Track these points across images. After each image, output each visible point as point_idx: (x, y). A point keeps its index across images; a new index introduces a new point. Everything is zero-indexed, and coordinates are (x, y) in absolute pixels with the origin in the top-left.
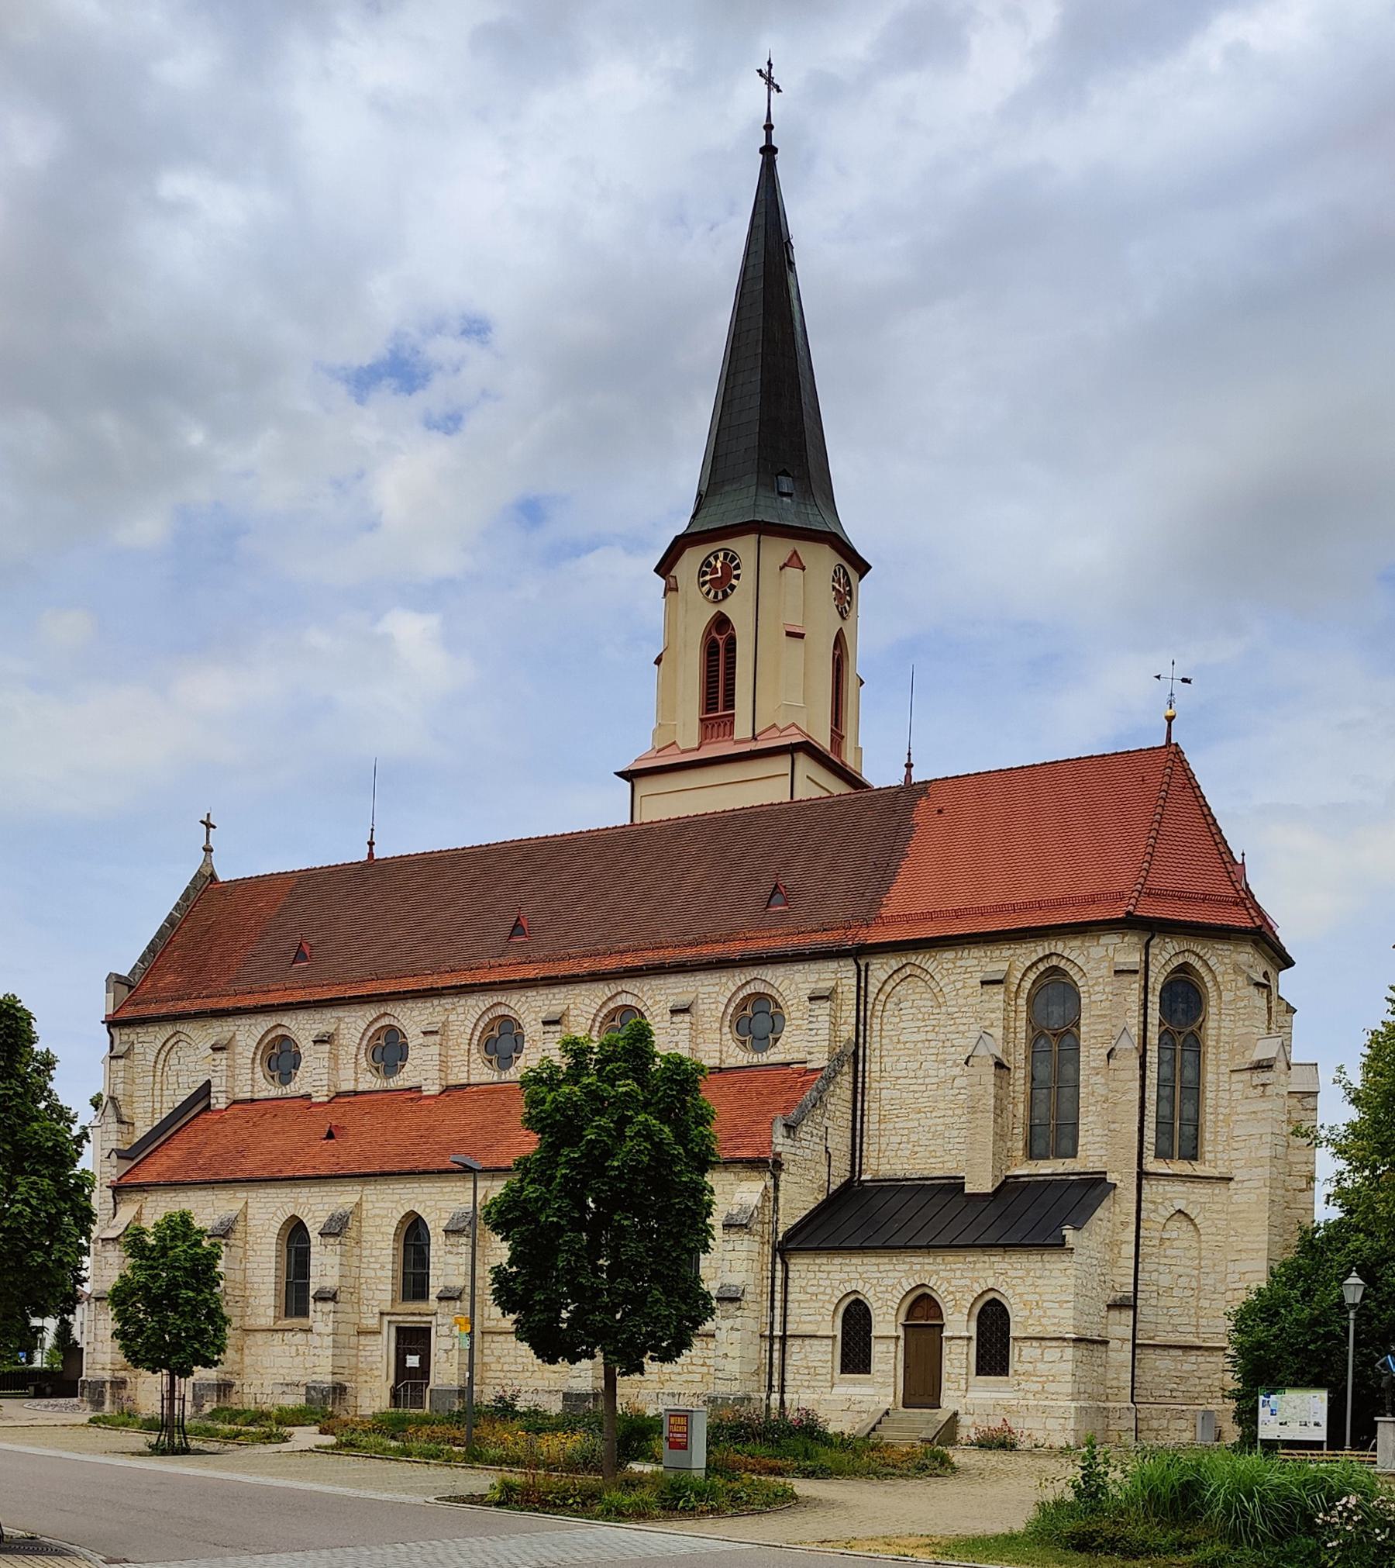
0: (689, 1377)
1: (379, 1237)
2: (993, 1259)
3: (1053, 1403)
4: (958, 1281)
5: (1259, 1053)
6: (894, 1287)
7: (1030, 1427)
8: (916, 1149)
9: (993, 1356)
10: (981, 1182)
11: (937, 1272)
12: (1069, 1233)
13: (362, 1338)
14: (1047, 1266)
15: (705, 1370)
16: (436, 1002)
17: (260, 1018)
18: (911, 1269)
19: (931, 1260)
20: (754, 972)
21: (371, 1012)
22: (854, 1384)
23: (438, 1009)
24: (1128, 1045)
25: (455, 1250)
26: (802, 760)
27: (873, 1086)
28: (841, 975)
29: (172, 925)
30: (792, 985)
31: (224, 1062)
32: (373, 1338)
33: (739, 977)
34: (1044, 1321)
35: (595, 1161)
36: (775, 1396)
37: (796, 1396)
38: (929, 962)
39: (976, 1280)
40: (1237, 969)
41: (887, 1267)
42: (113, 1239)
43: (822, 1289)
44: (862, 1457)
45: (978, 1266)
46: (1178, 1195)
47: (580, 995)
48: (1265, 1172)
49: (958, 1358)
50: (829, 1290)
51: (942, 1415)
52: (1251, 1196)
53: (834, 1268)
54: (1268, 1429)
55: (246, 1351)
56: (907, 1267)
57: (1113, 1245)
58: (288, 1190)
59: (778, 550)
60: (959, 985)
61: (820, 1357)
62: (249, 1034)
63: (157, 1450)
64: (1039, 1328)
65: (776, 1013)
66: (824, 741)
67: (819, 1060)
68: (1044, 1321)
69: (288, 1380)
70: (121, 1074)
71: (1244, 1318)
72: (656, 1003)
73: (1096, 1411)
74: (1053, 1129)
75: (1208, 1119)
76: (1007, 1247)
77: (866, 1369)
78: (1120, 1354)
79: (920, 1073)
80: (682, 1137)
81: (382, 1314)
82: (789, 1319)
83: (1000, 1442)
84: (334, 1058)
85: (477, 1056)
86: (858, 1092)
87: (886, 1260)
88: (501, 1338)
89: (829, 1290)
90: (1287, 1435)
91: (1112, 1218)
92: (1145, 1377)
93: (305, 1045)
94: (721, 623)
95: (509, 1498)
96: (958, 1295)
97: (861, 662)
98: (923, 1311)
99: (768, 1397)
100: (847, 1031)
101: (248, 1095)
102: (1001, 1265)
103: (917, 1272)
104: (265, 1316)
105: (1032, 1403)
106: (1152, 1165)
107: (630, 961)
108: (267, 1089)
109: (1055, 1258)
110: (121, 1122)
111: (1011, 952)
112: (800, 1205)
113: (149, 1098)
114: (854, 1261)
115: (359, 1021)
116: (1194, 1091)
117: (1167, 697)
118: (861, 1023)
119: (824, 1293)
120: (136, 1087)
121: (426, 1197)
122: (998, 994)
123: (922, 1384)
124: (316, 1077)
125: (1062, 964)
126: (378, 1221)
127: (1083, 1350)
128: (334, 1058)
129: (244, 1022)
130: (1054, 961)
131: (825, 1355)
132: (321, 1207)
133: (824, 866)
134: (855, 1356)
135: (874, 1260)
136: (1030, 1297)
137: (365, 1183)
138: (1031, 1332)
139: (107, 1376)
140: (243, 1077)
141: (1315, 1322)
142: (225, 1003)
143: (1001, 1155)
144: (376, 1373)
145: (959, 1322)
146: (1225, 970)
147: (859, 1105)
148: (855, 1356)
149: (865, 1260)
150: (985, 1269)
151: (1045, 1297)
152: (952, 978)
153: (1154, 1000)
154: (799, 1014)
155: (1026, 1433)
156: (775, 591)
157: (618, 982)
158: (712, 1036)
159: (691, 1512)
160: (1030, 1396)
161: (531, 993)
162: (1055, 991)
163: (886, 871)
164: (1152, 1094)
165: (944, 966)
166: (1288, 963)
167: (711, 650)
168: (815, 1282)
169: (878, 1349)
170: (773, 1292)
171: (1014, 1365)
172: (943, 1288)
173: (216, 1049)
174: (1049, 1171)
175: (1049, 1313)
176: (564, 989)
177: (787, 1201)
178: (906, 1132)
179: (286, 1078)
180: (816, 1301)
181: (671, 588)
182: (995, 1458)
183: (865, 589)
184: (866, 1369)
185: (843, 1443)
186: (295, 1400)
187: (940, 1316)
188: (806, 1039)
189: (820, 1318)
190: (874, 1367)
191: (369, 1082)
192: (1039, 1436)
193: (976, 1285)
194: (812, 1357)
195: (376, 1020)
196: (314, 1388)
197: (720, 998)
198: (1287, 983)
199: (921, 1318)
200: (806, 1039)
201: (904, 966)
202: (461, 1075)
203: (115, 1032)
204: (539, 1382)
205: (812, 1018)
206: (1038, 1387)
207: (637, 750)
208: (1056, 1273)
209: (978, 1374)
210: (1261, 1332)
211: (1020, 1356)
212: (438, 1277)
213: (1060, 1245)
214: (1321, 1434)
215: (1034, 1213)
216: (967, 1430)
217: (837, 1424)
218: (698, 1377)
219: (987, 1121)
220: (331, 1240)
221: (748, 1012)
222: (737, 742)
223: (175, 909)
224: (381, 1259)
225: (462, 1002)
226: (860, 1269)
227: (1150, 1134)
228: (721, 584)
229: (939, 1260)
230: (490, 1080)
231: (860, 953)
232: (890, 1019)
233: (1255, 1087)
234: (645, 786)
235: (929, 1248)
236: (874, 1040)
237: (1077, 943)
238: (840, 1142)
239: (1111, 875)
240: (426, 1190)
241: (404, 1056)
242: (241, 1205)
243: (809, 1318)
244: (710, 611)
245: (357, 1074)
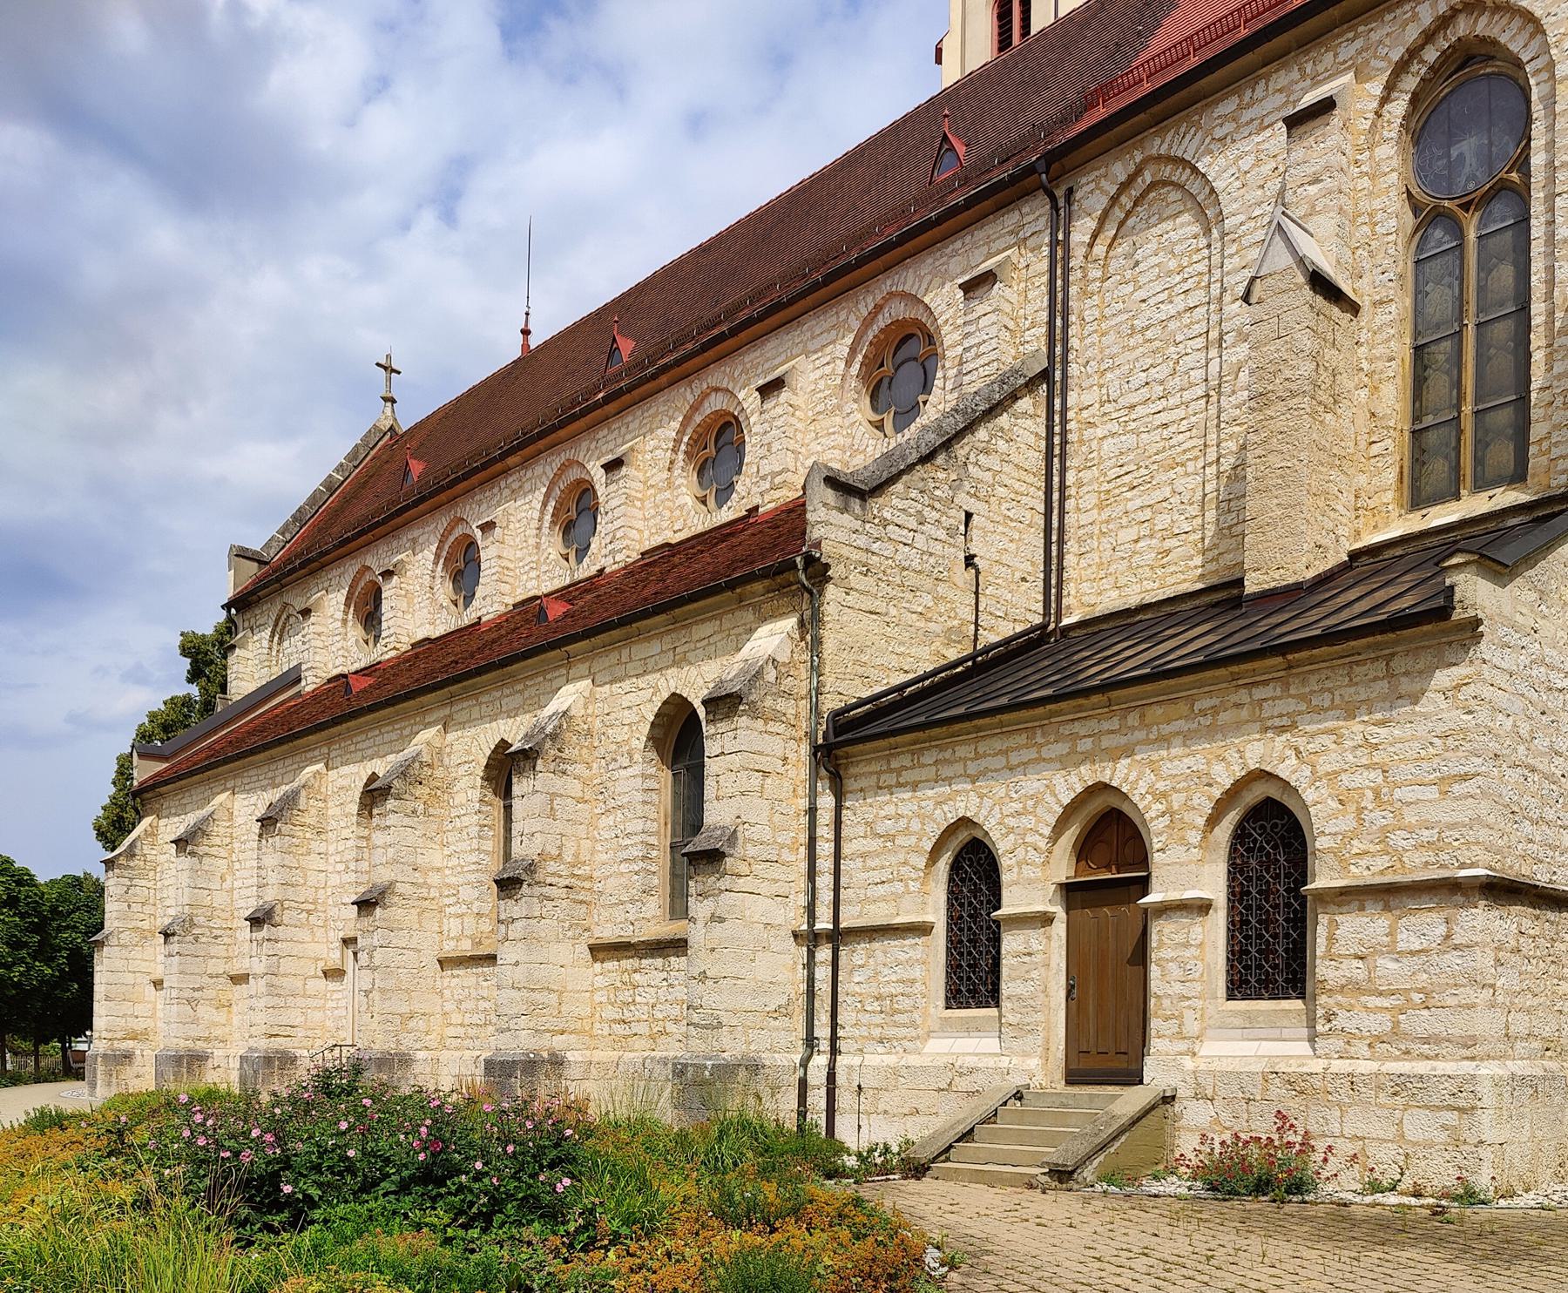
3: (1422, 1067)
8: (1168, 544)
9: (1271, 957)
18: (1073, 751)
19: (1115, 724)
36: (820, 1061)
37: (857, 1061)
43: (902, 823)
45: (1224, 717)
49: (1189, 958)
50: (915, 825)
64: (1382, 862)
68: (1398, 839)
82: (843, 894)
86: (1055, 451)
87: (1021, 739)
89: (915, 825)
96: (1177, 800)
99: (804, 1064)
105: (1365, 1067)
111: (1358, 44)
112: (895, 662)
119: (906, 832)
138: (1360, 874)
145: (1190, 868)
147: (1056, 479)
155: (1345, 1148)
170: (812, 841)
171: (1324, 969)
172: (1143, 787)
175: (1410, 817)
177: (842, 647)
178: (1148, 514)
184: (992, 996)
187: (1143, 860)
189: (900, 887)
190: (1006, 989)
201: (1139, 171)
206: (1378, 1024)
211: (1339, 943)
221: (888, 367)
223: (337, 470)
225: (529, 474)
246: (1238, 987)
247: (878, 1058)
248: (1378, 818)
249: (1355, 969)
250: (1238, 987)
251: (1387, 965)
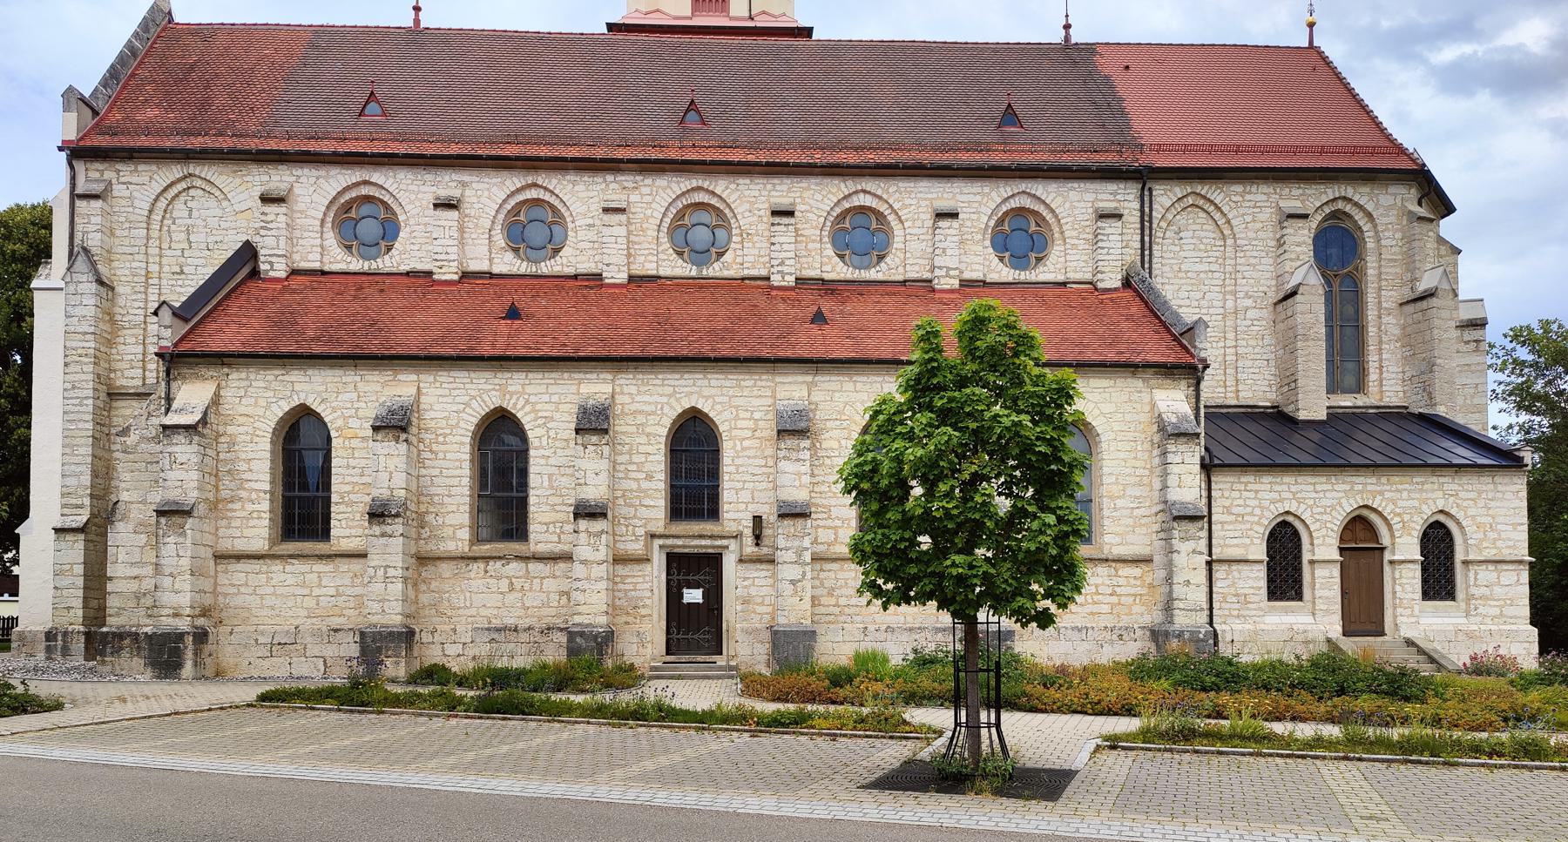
0: (1095, 609)
1: (643, 439)
2: (1442, 480)
3: (1514, 627)
6: (1333, 508)
9: (1439, 578)
11: (1381, 493)
13: (619, 568)
14: (1500, 488)
15: (1114, 599)
16: (610, 178)
17: (334, 171)
20: (1023, 185)
21: (513, 181)
22: (1286, 611)
23: (612, 186)
25: (794, 455)
28: (1124, 197)
29: (134, 55)
30: (1072, 205)
31: (282, 218)
32: (637, 567)
34: (1499, 544)
39: (1425, 501)
41: (1326, 487)
42: (187, 427)
43: (1249, 510)
47: (808, 189)
53: (1263, 487)
55: (423, 587)
56: (1348, 487)
58: (487, 375)
60: (1248, 218)
61: (1251, 583)
64: (1494, 552)
65: (1037, 232)
68: (1499, 544)
69: (496, 623)
70: (98, 219)
72: (906, 206)
77: (1451, 595)
79: (1203, 302)
81: (653, 536)
87: (1324, 479)
88: (835, 566)
96: (1406, 517)
98: (1361, 539)
101: (316, 265)
102: (1452, 486)
103: (1360, 492)
104: (454, 538)
109: (1507, 480)
110: (100, 282)
113: (141, 257)
114: (1287, 479)
115: (495, 190)
117: (1307, 7)
118: (1146, 249)
119: (1252, 514)
120: (117, 241)
121: (714, 391)
123: (1363, 607)
124: (439, 249)
125: (1348, 208)
126: (640, 419)
130: (1340, 205)
132: (546, 398)
135: (1310, 479)
136: (1483, 520)
137: (620, 371)
139: (183, 625)
144: (643, 612)
145: (1405, 547)
149: (1300, 479)
150: (1433, 491)
151: (1500, 519)
152: (1241, 211)
154: (1075, 233)
157: (857, 180)
158: (974, 248)
160: (1488, 620)
161: (743, 181)
168: (1241, 502)
173: (266, 199)
174: (1349, 404)
175: (1503, 535)
176: (787, 181)
180: (1243, 522)
184: (1451, 595)
185: (1048, 682)
186: (554, 653)
189: (1248, 541)
193: (1424, 507)
194: (1241, 584)
195: (518, 191)
196: (582, 634)
197: (983, 209)
199: (1365, 541)
202: (648, 266)
203: (80, 166)
208: (1509, 496)
212: (737, 491)
218: (1106, 609)
220: (594, 439)
222: (731, 19)
224: (647, 467)
226: (1293, 488)
229: (1384, 480)
230: (687, 274)
233: (1467, 342)
237: (1365, 189)
240: (713, 383)
242: (413, 391)
243: (1235, 541)
246: (1426, 595)
247: (1238, 626)
248: (1492, 535)
249: (1483, 590)
250: (1426, 595)
251: (1497, 589)
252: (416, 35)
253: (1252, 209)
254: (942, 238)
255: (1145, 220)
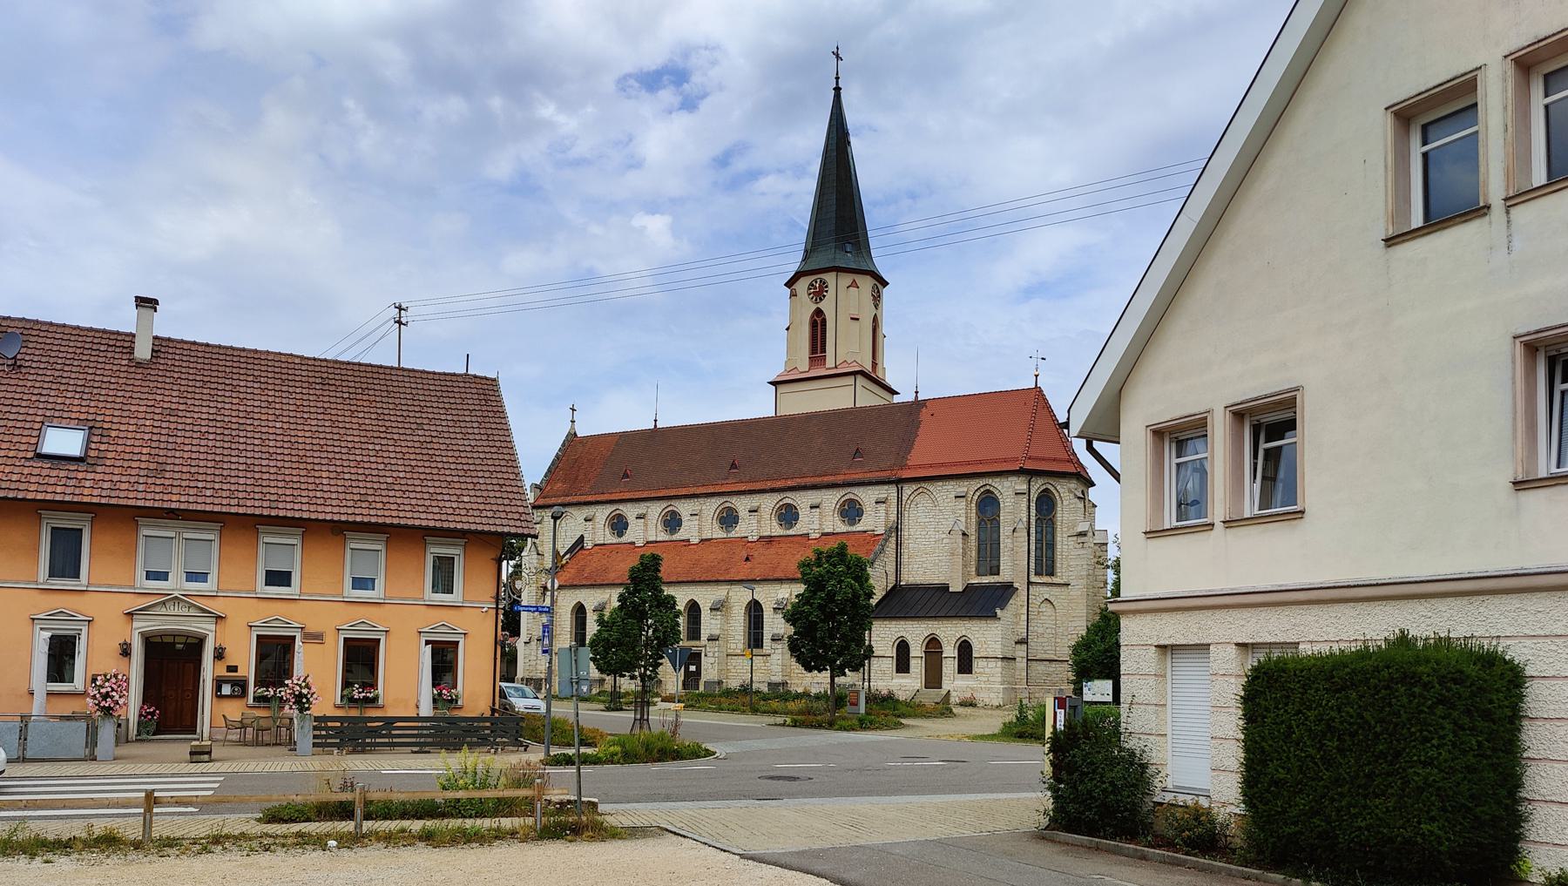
4: (950, 633)
5: (1080, 529)
7: (983, 697)
9: (966, 662)
10: (957, 586)
12: (998, 611)
21: (664, 504)
24: (1022, 526)
26: (859, 378)
27: (905, 543)
28: (890, 492)
30: (867, 496)
33: (842, 492)
35: (831, 597)
38: (930, 486)
40: (1070, 491)
44: (913, 709)
46: (1046, 592)
48: (1084, 582)
49: (950, 666)
51: (943, 692)
52: (1078, 591)
54: (1088, 697)
57: (1017, 615)
59: (846, 279)
62: (602, 514)
63: (608, 709)
66: (868, 367)
67: (880, 531)
71: (1076, 649)
73: (1011, 690)
74: (988, 556)
75: (1058, 557)
76: (971, 617)
78: (1021, 664)
80: (861, 586)
83: (969, 703)
84: (646, 525)
85: (716, 525)
86: (899, 545)
90: (1095, 699)
91: (1017, 603)
92: (1032, 674)
93: (631, 518)
94: (819, 312)
95: (795, 724)
97: (885, 328)
98: (933, 645)
100: (893, 517)
106: (1034, 579)
107: (790, 483)
108: (611, 539)
116: (1052, 546)
118: (899, 514)
122: (963, 503)
123: (933, 678)
127: (1005, 663)
128: (646, 525)
129: (599, 507)
131: (890, 665)
133: (882, 441)
134: (903, 665)
140: (599, 533)
141: (1106, 651)
142: (590, 499)
143: (965, 575)
145: (950, 650)
146: (1064, 492)
148: (903, 665)
153: (1033, 505)
156: (845, 297)
159: (869, 729)
162: (988, 505)
163: (908, 444)
164: (1033, 547)
165: (937, 489)
166: (1093, 484)
167: (814, 324)
169: (913, 662)
179: (620, 535)
181: (793, 295)
182: (969, 710)
183: (886, 291)
185: (907, 704)
188: (874, 520)
191: (663, 536)
192: (987, 701)
198: (1093, 494)
200: (874, 520)
204: (818, 682)
205: (877, 511)
207: (777, 370)
209: (289, 585)
210: (1084, 655)
213: (995, 616)
214: (1110, 699)
215: (984, 601)
216: (954, 699)
217: (902, 696)
219: (959, 559)
227: (1032, 565)
228: (819, 293)
231: (899, 482)
232: (913, 512)
234: (782, 389)
235: (935, 617)
236: (905, 521)
238: (891, 568)
239: (1013, 449)
241: (680, 525)
244: (814, 307)
245: (657, 533)
252: (656, 431)
253: (945, 492)
254: (819, 516)
255: (899, 499)
